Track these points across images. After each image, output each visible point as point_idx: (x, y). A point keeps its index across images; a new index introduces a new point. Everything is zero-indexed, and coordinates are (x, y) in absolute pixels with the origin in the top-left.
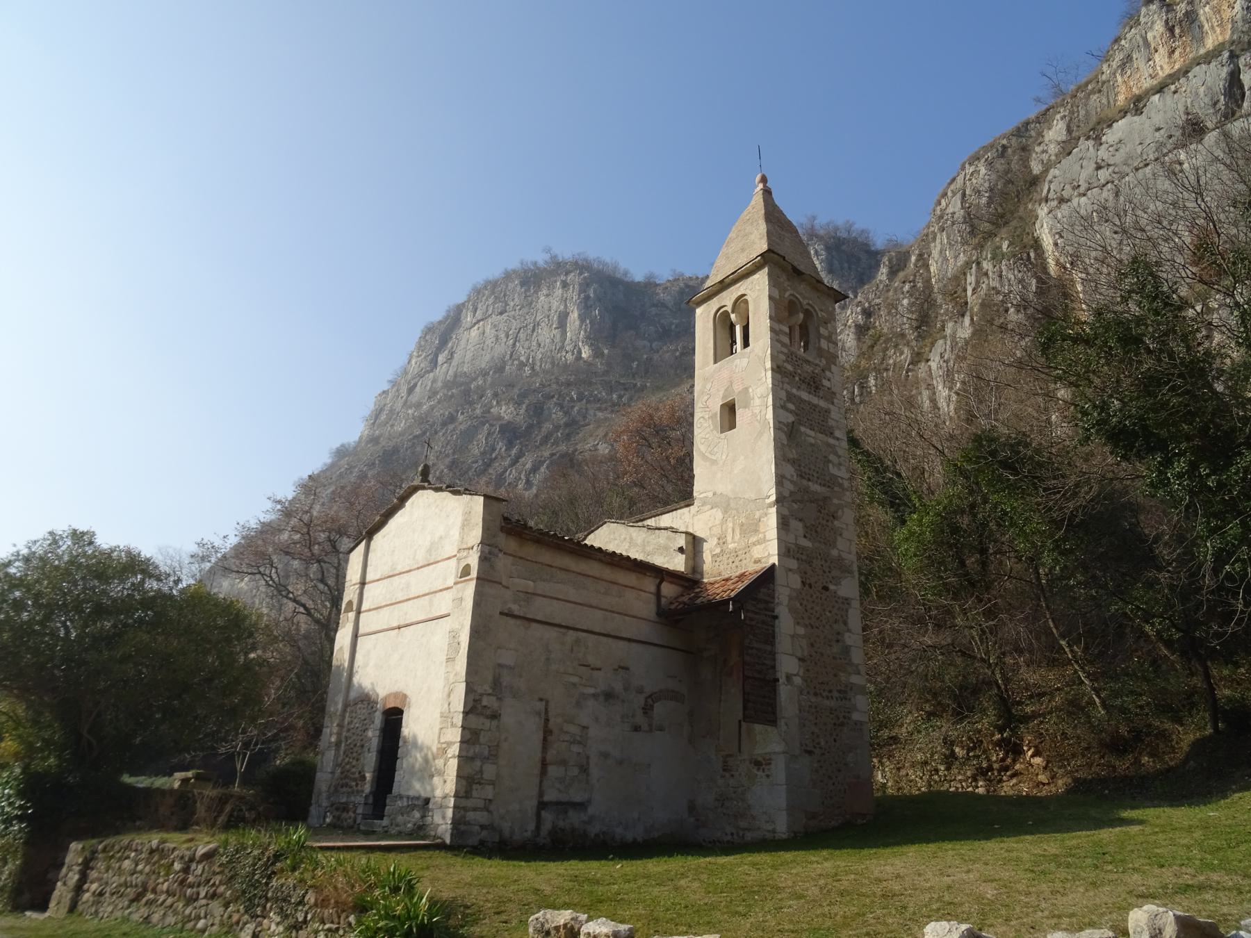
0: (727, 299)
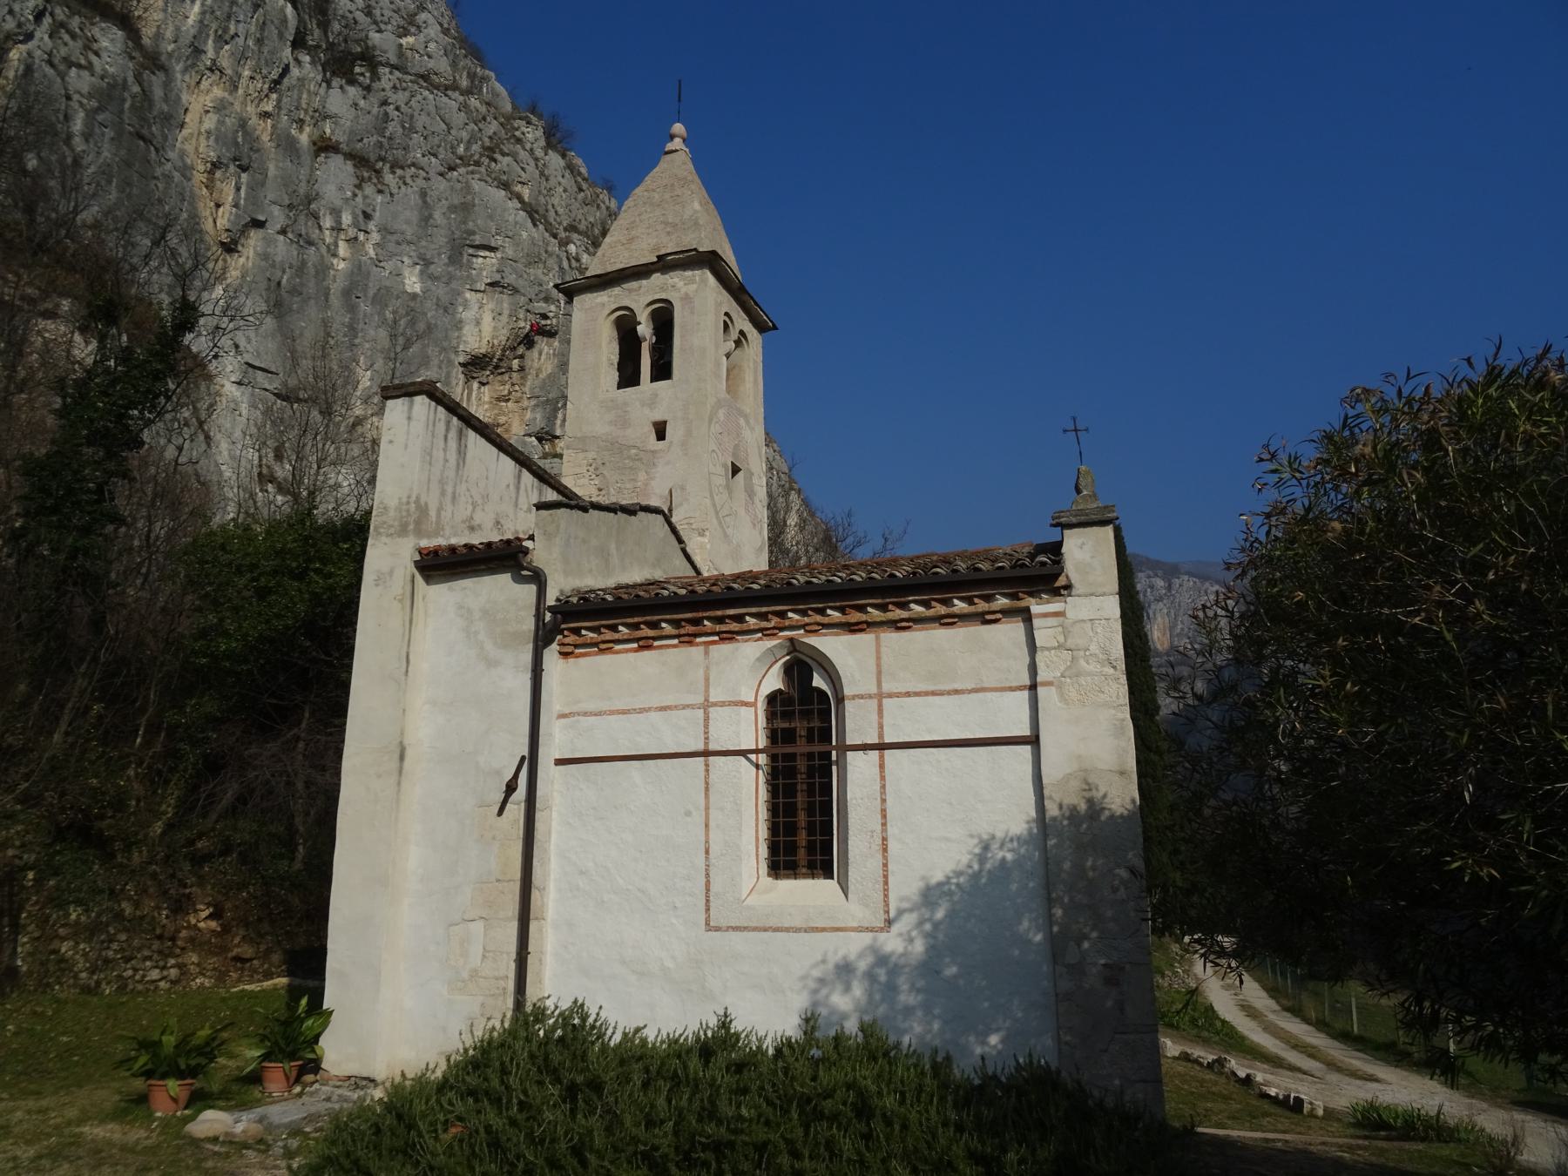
0: (639, 297)
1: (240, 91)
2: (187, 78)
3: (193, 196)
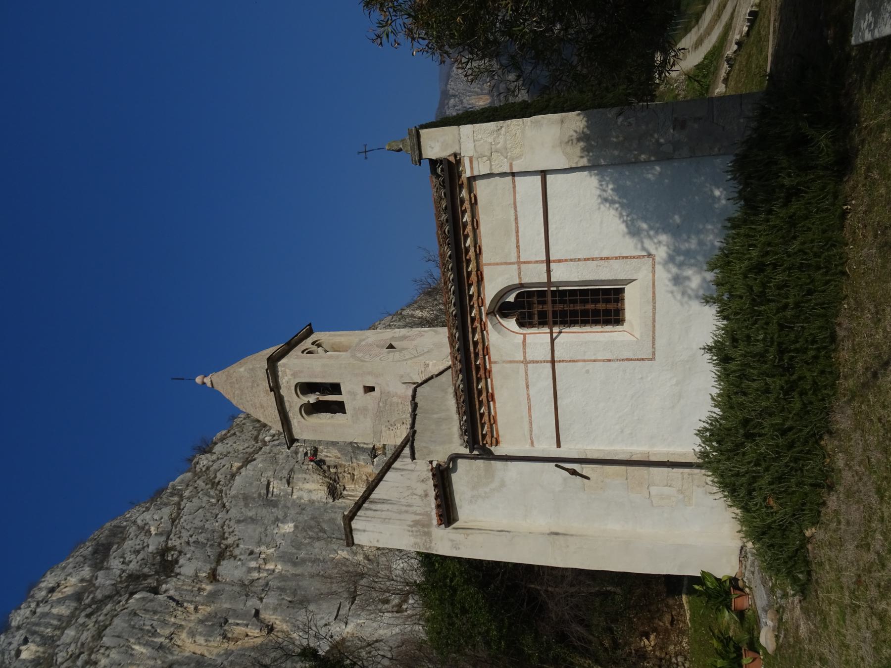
1: (183, 623)
2: (176, 653)
3: (241, 649)
